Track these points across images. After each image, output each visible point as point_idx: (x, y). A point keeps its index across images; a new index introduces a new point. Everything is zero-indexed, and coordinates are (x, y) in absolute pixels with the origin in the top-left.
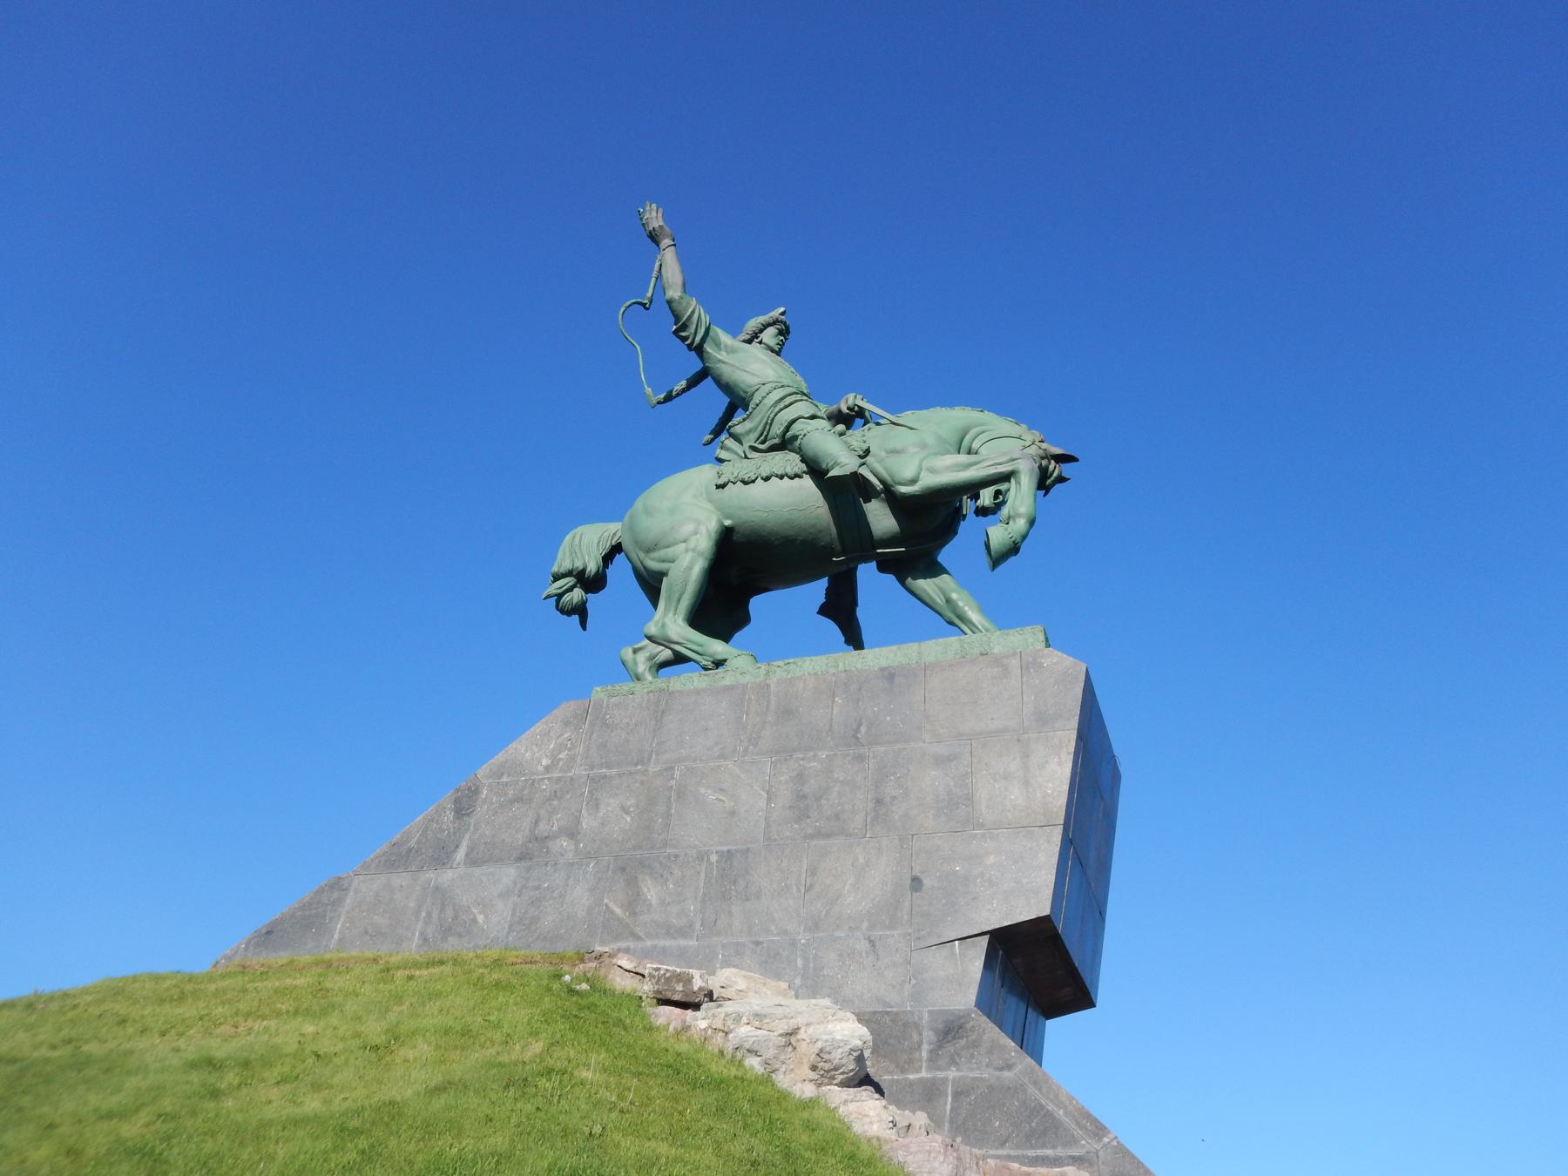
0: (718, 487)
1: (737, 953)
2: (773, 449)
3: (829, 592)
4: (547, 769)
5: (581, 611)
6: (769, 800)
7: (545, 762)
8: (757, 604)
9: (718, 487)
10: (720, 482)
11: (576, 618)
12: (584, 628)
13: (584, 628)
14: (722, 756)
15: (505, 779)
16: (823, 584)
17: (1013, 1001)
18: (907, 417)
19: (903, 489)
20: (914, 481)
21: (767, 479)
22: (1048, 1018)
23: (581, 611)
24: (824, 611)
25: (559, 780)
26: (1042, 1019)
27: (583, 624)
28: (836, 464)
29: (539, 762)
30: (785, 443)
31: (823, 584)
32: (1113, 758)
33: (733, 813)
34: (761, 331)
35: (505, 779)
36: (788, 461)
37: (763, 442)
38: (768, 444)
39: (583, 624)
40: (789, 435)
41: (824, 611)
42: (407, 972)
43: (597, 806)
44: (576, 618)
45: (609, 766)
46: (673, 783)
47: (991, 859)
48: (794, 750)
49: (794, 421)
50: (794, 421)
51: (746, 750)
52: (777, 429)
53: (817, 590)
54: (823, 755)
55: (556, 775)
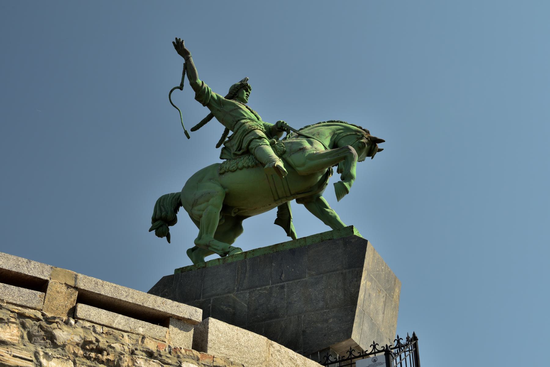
0: (221, 174)
2: (243, 154)
3: (279, 214)
8: (245, 223)
9: (221, 174)
10: (222, 171)
11: (165, 238)
13: (384, 141)
14: (229, 292)
20: (303, 165)
24: (277, 222)
27: (169, 240)
37: (240, 150)
38: (241, 151)
39: (169, 240)
40: (250, 147)
41: (277, 222)
44: (165, 238)
46: (210, 305)
47: (331, 320)
48: (257, 287)
49: (251, 141)
50: (251, 141)
51: (238, 288)
52: (245, 145)
53: (273, 213)
54: (268, 287)
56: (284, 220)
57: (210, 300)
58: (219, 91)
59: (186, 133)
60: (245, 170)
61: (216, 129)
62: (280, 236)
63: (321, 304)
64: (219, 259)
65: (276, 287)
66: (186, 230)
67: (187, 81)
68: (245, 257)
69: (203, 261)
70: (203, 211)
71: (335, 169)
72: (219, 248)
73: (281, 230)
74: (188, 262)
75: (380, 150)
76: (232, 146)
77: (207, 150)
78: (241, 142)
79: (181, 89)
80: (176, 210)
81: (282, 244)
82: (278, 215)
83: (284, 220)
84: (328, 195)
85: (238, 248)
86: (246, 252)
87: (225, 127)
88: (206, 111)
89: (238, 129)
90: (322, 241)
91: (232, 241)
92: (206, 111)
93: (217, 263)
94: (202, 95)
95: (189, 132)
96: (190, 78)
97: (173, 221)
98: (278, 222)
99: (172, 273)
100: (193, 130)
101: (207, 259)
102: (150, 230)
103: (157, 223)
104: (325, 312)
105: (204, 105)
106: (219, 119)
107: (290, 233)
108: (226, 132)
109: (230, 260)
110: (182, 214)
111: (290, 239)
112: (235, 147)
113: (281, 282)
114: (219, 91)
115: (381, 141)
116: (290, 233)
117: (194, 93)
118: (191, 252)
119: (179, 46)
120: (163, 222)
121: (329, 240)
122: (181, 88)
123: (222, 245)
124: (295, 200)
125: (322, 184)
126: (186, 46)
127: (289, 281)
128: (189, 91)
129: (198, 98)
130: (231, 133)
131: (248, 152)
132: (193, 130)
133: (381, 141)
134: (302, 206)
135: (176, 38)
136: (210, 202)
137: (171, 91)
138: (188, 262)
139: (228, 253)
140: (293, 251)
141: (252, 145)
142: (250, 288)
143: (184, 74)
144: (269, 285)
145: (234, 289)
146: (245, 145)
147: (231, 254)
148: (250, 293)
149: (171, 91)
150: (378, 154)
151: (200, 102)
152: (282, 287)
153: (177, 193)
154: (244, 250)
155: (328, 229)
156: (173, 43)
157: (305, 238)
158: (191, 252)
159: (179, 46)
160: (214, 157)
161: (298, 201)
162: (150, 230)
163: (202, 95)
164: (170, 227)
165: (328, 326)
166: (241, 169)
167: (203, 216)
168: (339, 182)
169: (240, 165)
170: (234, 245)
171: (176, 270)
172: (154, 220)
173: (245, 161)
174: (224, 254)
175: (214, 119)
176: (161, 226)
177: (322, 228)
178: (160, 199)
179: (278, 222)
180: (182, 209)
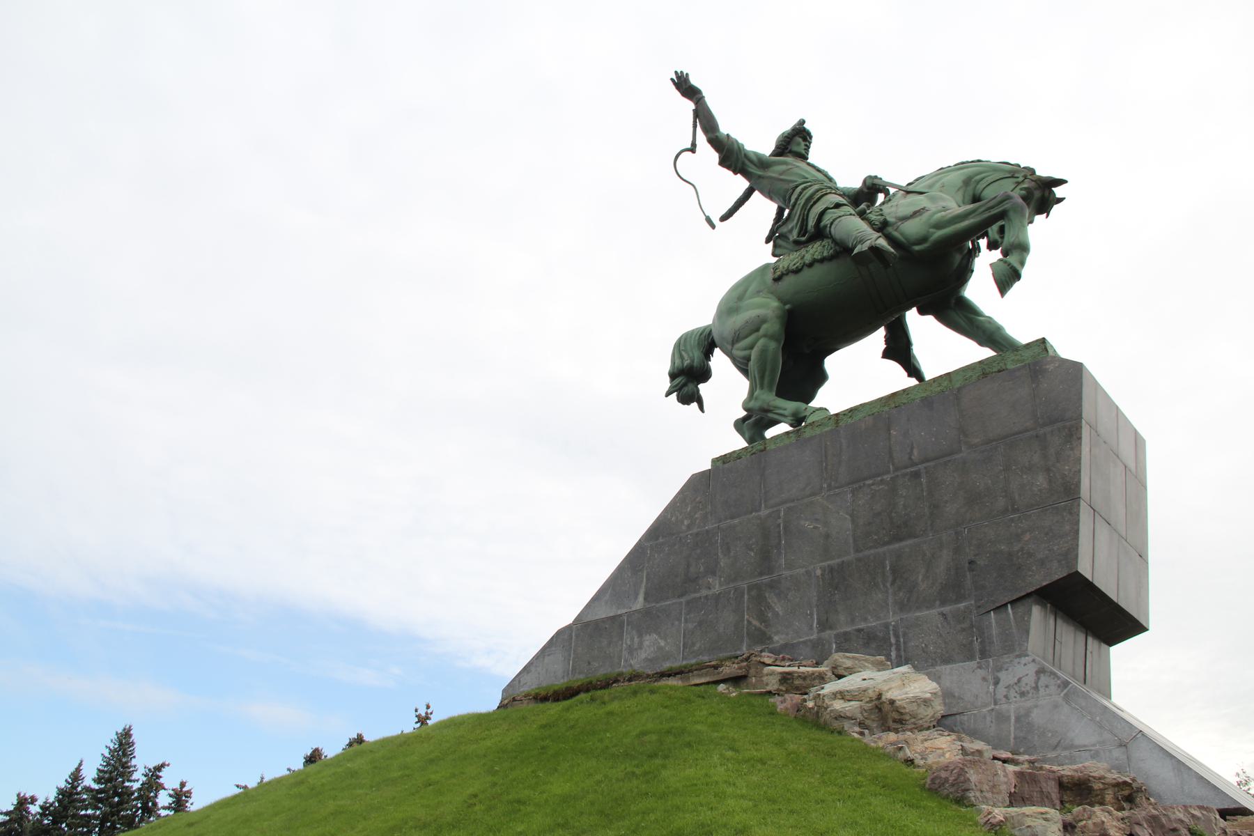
1: (846, 640)
3: (888, 340)
4: (689, 527)
6: (853, 521)
7: (686, 522)
8: (832, 363)
11: (695, 405)
14: (813, 494)
15: (661, 540)
16: (881, 333)
19: (917, 248)
22: (1111, 643)
24: (887, 354)
25: (697, 534)
26: (1104, 646)
27: (701, 408)
29: (682, 522)
31: (881, 333)
33: (827, 536)
35: (661, 540)
39: (701, 408)
40: (822, 224)
41: (887, 354)
42: (1016, 757)
43: (728, 549)
44: (695, 405)
45: (732, 518)
46: (780, 521)
47: (1027, 537)
48: (866, 479)
49: (822, 214)
51: (829, 485)
52: (811, 223)
53: (877, 339)
54: (887, 477)
55: (695, 530)
56: (899, 349)
57: (779, 511)
58: (760, 141)
59: (709, 221)
60: (817, 265)
61: (762, 210)
62: (895, 379)
63: (1001, 503)
64: (787, 433)
65: (904, 475)
66: (728, 386)
67: (701, 138)
68: (837, 422)
69: (764, 438)
71: (983, 243)
72: (786, 413)
73: (895, 368)
74: (739, 443)
75: (1060, 200)
76: (791, 231)
77: (747, 243)
78: (804, 221)
80: (708, 353)
81: (904, 391)
82: (887, 342)
83: (899, 349)
84: (979, 288)
85: (821, 409)
86: (837, 415)
89: (797, 199)
90: (985, 375)
91: (809, 397)
92: (741, 184)
93: (787, 441)
94: (732, 156)
95: (716, 220)
96: (705, 131)
97: (705, 375)
99: (708, 466)
100: (724, 218)
101: (770, 433)
102: (668, 394)
103: (677, 381)
104: (1012, 520)
106: (762, 192)
107: (912, 369)
108: (780, 211)
109: (808, 433)
110: (720, 362)
111: (913, 382)
112: (795, 233)
113: (912, 466)
114: (760, 141)
115: (1061, 182)
116: (912, 369)
117: (715, 156)
118: (740, 425)
119: (684, 86)
120: (688, 379)
121: (999, 371)
122: (693, 149)
123: (790, 406)
124: (915, 309)
125: (964, 273)
126: (694, 81)
127: (928, 461)
129: (724, 162)
130: (787, 212)
131: (820, 233)
132: (724, 218)
133: (1061, 182)
134: (930, 319)
136: (762, 331)
138: (739, 443)
139: (803, 419)
140: (927, 402)
141: (826, 220)
142: (853, 483)
143: (695, 127)
144: (888, 472)
145: (822, 488)
146: (811, 223)
147: (809, 420)
148: (853, 492)
150: (1056, 209)
151: (728, 167)
152: (916, 475)
153: (705, 328)
154: (833, 411)
155: (987, 353)
157: (948, 374)
158: (740, 425)
159: (684, 86)
160: (764, 255)
161: (922, 312)
162: (668, 394)
164: (701, 386)
165: (1022, 549)
166: (810, 265)
167: (753, 358)
168: (1000, 260)
169: (808, 258)
170: (815, 403)
171: (714, 461)
172: (673, 376)
173: (816, 250)
174: (797, 420)
175: (756, 194)
176: (685, 385)
177: (968, 352)
178: (680, 339)
180: (717, 351)
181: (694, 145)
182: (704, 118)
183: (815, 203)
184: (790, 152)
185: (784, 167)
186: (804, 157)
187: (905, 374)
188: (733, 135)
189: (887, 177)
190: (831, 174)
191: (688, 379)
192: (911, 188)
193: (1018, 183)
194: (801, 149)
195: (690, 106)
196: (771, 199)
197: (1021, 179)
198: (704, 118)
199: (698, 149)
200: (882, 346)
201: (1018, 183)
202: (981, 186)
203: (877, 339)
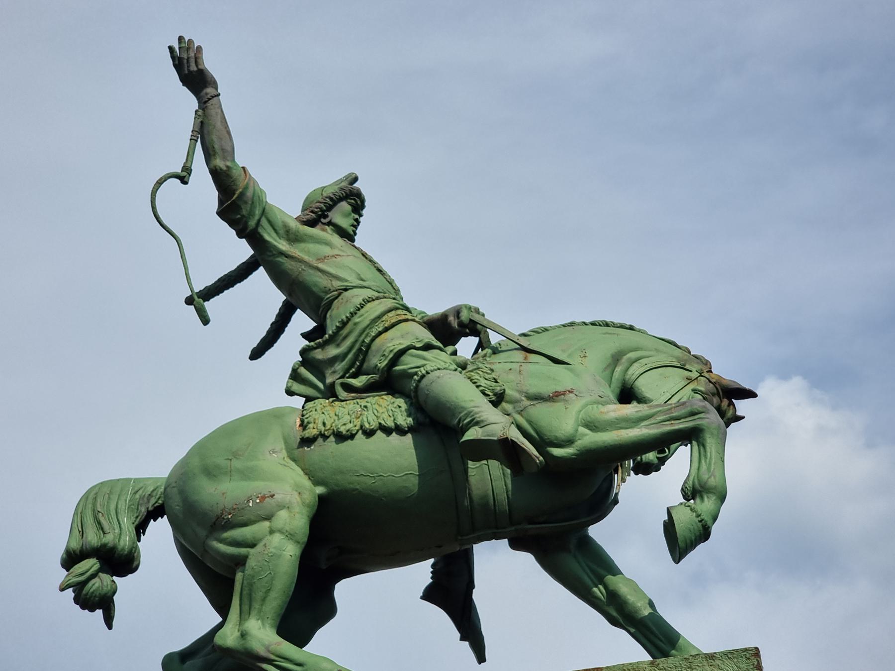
5: (103, 604)
11: (99, 613)
12: (110, 626)
13: (110, 626)
16: (432, 561)
17: (306, 518)
18: (225, 168)
21: (369, 433)
23: (103, 604)
24: (430, 595)
27: (109, 621)
28: (475, 423)
30: (390, 381)
32: (238, 267)
34: (330, 208)
36: (390, 409)
39: (109, 621)
41: (430, 595)
44: (99, 613)
49: (402, 352)
52: (378, 361)
53: (421, 573)
70: (253, 546)
79: (184, 181)
87: (252, 252)
88: (244, 251)
92: (244, 251)
94: (237, 205)
96: (209, 155)
98: (432, 595)
105: (240, 235)
112: (340, 367)
117: (213, 194)
120: (98, 568)
126: (211, 63)
128: (204, 190)
134: (527, 559)
135: (181, 39)
137: (160, 183)
143: (193, 140)
149: (160, 183)
151: (232, 223)
156: (171, 49)
159: (194, 77)
163: (237, 205)
179: (432, 595)
181: (187, 169)
182: (209, 134)
183: (386, 330)
184: (330, 223)
185: (327, 250)
186: (348, 236)
187: (458, 635)
188: (253, 172)
189: (492, 314)
190: (398, 283)
191: (98, 568)
192: (524, 342)
193: (690, 380)
194: (345, 223)
195: (191, 102)
196: (280, 287)
197: (695, 375)
198: (209, 134)
199: (192, 179)
200: (427, 580)
201: (690, 380)
202: (635, 370)
203: (421, 573)
